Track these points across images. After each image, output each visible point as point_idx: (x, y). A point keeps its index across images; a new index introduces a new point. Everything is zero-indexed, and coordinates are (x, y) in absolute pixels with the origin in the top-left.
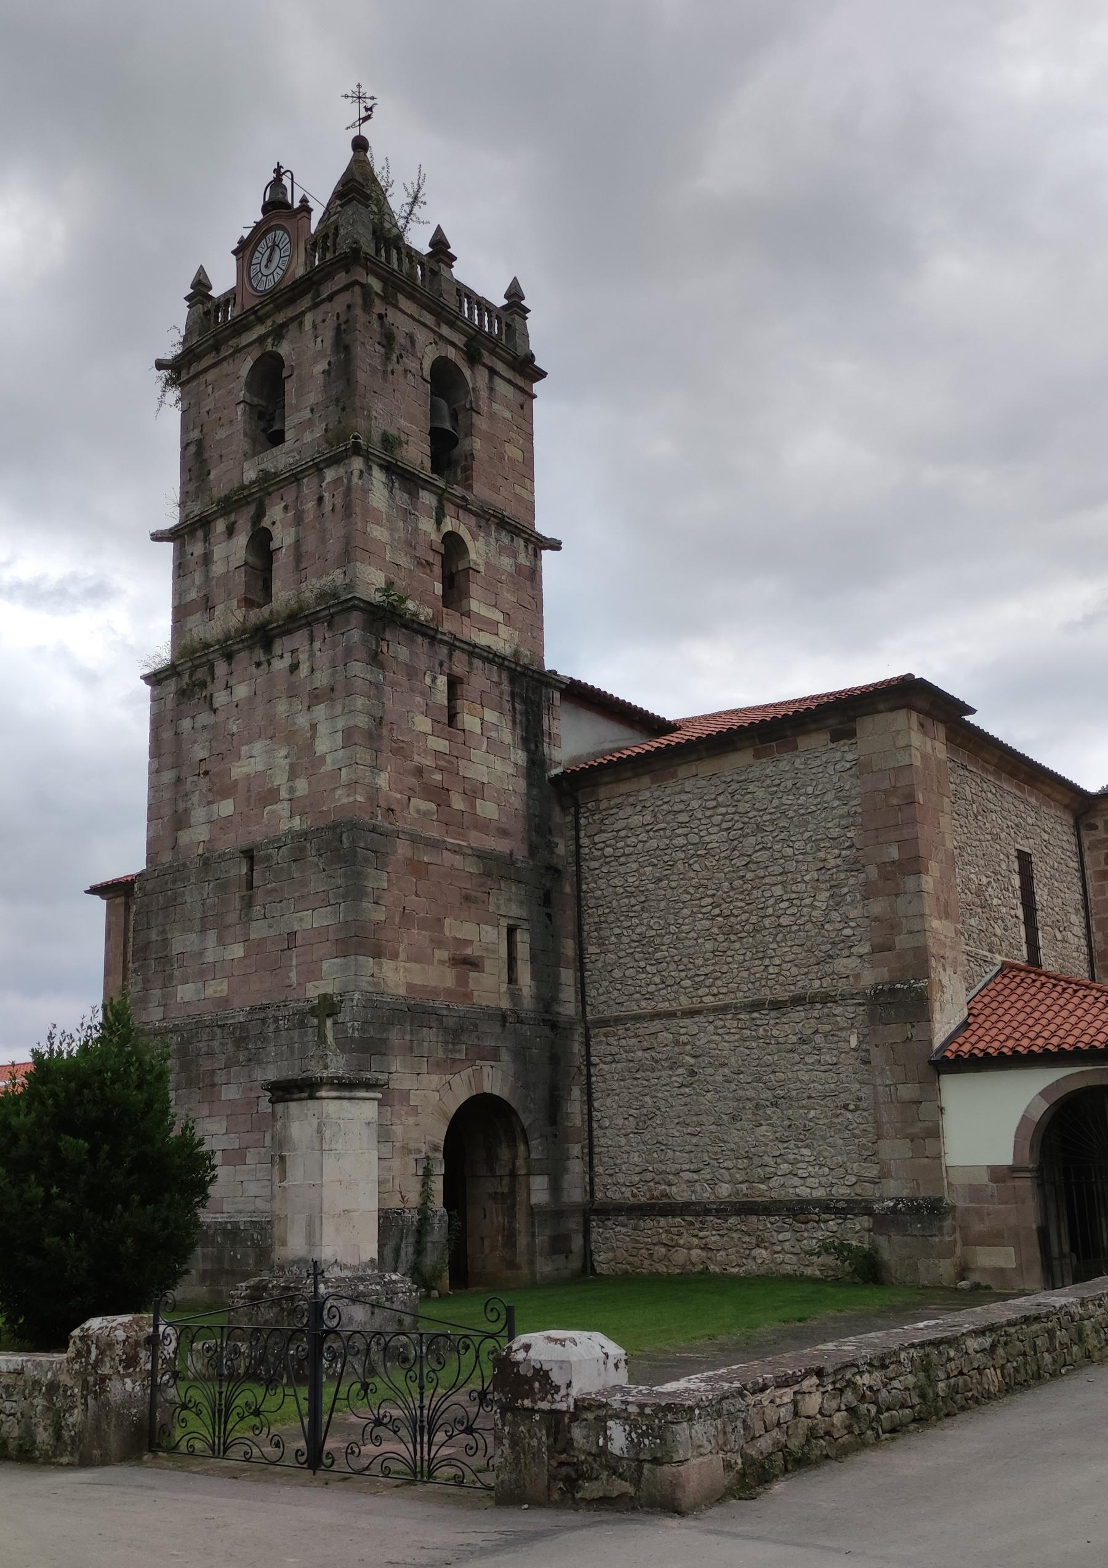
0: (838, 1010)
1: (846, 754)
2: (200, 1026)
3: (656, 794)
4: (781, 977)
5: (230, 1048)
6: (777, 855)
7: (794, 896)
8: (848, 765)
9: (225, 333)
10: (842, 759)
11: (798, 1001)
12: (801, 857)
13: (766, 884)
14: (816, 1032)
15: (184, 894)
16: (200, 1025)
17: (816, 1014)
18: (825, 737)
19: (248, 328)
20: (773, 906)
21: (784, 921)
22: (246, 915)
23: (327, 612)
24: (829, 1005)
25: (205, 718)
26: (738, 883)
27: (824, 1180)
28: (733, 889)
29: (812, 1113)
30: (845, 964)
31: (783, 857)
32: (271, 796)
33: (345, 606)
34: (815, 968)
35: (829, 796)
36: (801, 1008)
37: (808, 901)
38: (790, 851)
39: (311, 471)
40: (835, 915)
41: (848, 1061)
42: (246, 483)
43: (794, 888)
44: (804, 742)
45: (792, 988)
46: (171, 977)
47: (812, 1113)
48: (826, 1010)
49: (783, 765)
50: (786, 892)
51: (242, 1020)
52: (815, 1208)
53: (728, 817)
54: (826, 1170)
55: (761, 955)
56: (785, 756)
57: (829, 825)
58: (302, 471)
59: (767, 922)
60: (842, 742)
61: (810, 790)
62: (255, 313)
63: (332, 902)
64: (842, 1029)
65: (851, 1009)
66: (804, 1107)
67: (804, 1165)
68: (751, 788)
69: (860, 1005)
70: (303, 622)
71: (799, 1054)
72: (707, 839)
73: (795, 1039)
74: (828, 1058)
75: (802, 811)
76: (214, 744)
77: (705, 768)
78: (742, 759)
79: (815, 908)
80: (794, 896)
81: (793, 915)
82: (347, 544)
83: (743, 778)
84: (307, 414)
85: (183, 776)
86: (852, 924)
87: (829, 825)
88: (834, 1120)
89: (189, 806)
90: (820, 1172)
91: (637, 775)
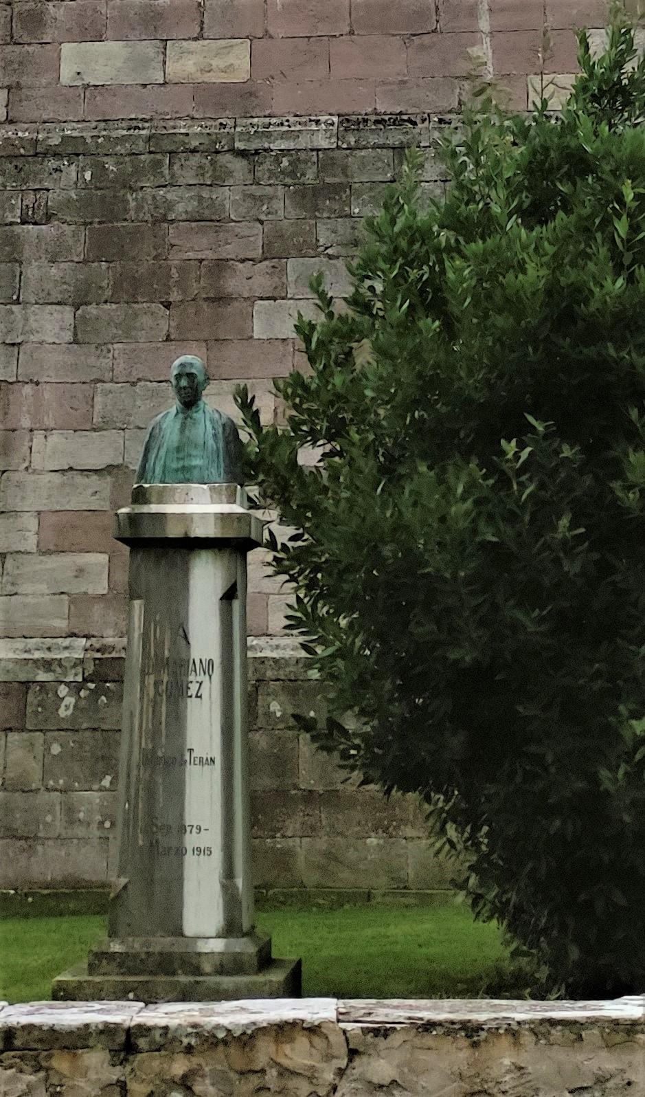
2: (165, 149)
5: (283, 210)
16: (167, 145)
51: (324, 144)
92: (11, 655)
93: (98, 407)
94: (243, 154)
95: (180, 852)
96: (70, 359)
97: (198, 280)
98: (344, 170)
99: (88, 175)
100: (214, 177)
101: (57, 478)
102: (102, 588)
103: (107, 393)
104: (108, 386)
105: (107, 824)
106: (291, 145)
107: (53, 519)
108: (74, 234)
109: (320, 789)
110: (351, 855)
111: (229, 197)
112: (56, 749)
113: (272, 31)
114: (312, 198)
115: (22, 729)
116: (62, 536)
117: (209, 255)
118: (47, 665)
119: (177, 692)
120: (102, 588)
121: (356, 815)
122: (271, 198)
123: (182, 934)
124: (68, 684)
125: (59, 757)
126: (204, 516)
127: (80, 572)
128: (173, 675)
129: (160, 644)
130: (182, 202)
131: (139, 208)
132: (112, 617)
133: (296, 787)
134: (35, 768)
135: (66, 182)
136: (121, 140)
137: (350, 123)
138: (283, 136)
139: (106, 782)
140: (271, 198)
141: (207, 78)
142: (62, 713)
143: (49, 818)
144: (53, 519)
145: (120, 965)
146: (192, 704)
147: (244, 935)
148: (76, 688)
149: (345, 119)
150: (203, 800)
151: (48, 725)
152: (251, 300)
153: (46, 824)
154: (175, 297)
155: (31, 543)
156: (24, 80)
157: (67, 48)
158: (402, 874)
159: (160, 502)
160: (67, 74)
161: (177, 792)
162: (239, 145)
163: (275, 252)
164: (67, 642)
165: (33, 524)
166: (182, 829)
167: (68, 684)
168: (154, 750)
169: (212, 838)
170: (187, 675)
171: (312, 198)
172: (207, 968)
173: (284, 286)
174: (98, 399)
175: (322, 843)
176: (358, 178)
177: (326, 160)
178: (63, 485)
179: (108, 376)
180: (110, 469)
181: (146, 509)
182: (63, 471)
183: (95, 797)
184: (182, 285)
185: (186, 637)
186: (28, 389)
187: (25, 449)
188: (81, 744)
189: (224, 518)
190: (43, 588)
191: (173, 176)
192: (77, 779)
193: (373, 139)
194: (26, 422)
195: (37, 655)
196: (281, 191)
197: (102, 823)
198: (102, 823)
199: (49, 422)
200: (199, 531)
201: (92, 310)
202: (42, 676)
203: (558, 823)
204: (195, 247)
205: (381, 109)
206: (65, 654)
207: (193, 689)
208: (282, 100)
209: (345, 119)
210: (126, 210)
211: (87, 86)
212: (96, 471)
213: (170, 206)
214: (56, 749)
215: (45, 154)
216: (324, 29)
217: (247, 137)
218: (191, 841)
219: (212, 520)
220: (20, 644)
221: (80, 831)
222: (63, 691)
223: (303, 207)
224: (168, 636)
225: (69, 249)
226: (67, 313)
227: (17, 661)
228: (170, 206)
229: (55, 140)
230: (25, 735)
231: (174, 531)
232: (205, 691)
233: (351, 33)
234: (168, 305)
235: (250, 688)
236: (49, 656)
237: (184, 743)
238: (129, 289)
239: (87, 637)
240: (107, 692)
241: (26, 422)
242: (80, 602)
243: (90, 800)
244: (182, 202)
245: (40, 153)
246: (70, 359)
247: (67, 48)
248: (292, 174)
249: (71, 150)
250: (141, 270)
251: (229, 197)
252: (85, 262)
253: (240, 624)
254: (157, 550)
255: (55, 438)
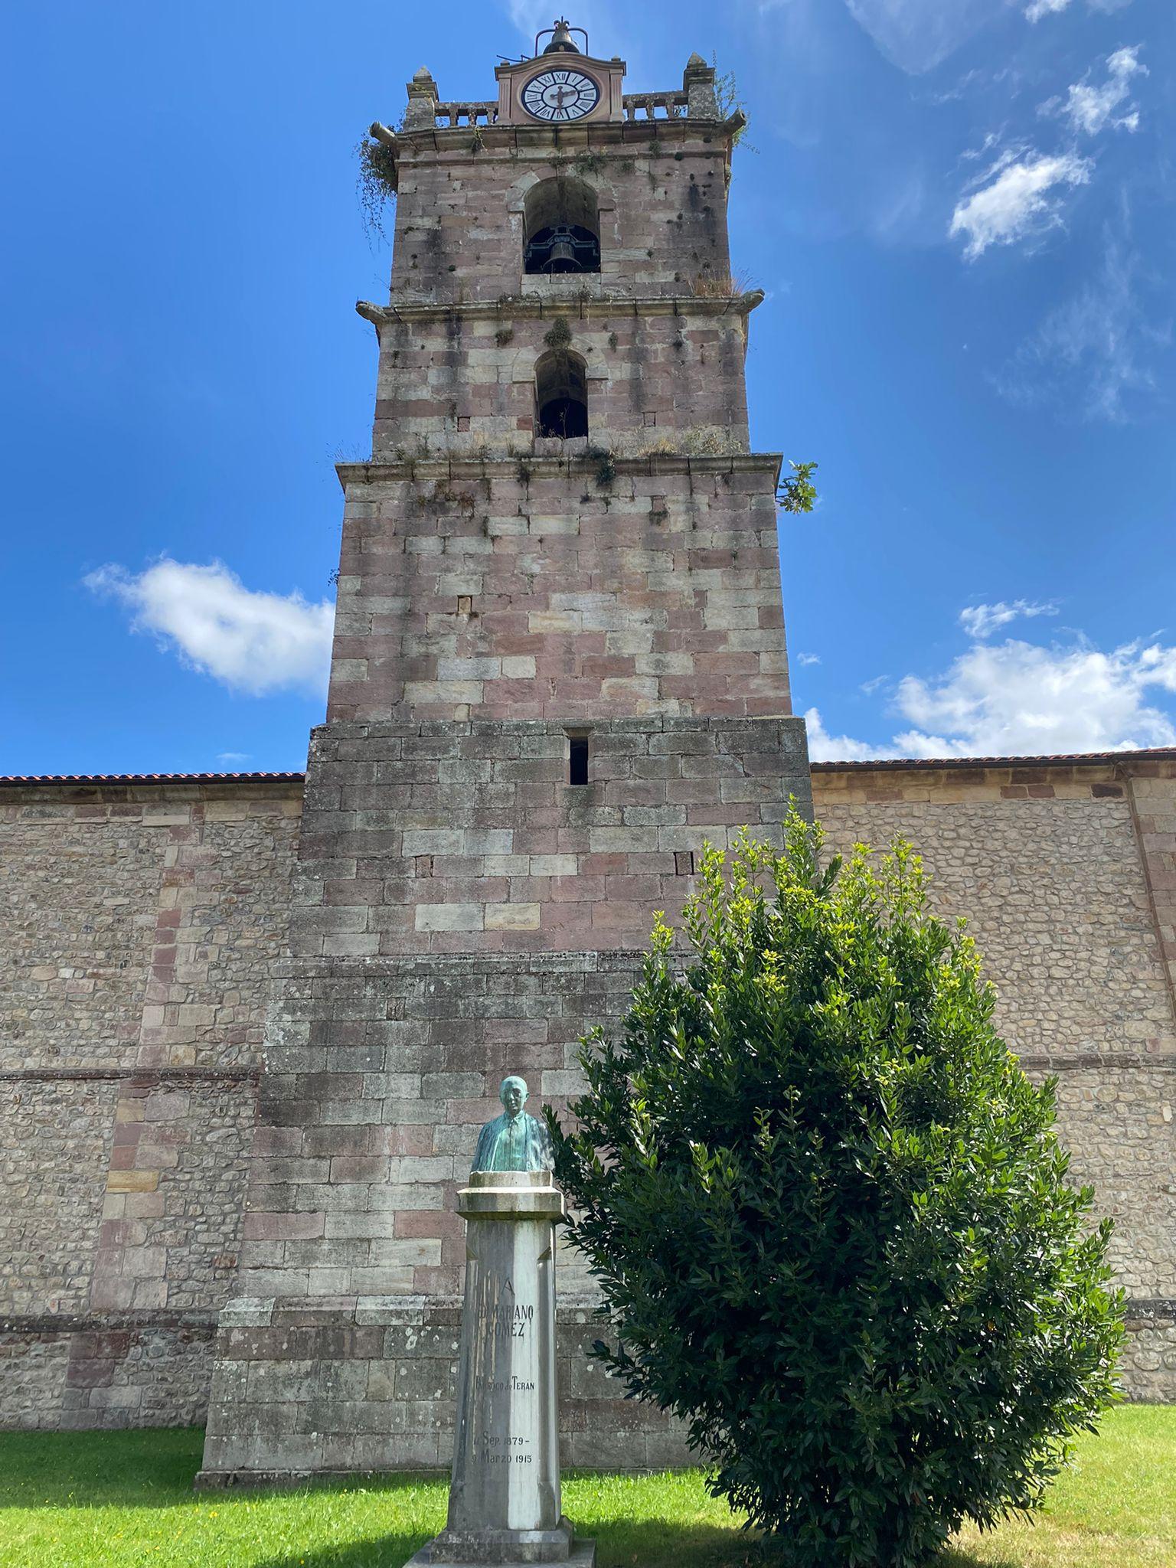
0: (1143, 1078)
1: (1112, 811)
2: (484, 970)
3: (874, 812)
4: (1059, 1035)
5: (562, 1012)
6: (1040, 901)
7: (1067, 947)
8: (1116, 823)
9: (498, 136)
10: (1109, 816)
11: (1091, 1061)
12: (1070, 908)
13: (1029, 930)
14: (1117, 1100)
15: (433, 770)
16: (485, 969)
17: (1115, 1079)
18: (1087, 791)
19: (532, 143)
20: (1040, 955)
21: (1056, 972)
22: (581, 816)
23: (728, 464)
24: (1131, 1070)
25: (467, 543)
26: (991, 925)
27: (1147, 1277)
28: (984, 930)
29: (1123, 1196)
30: (1135, 1028)
31: (1047, 904)
32: (623, 666)
33: (761, 463)
34: (1103, 1029)
35: (1096, 850)
36: (1095, 1071)
37: (1084, 955)
38: (1055, 899)
39: (665, 311)
40: (1119, 974)
41: (1162, 1136)
42: (524, 293)
43: (1065, 938)
44: (1061, 791)
45: (1075, 1048)
46: (399, 891)
47: (1123, 1196)
48: (1127, 1077)
49: (1037, 809)
50: (1055, 942)
51: (588, 969)
52: (1148, 1311)
53: (974, 852)
54: (1149, 1264)
55: (1031, 1007)
56: (1040, 800)
57: (1101, 879)
58: (648, 307)
59: (1035, 972)
60: (1107, 799)
61: (1074, 840)
62: (556, 131)
63: (766, 819)
64: (1149, 1099)
65: (1159, 1078)
66: (1111, 1187)
67: (1119, 1258)
68: (1001, 825)
69: (1168, 1073)
70: (681, 466)
71: (1098, 1125)
72: (949, 870)
73: (1090, 1106)
74: (1136, 1130)
75: (1065, 860)
76: (492, 581)
77: (941, 796)
78: (988, 794)
79: (1093, 963)
80: (1067, 947)
81: (1068, 967)
82: (731, 402)
83: (989, 813)
84: (642, 255)
85: (420, 608)
86: (1141, 985)
87: (1101, 879)
88: (1152, 1204)
89: (434, 649)
90: (1141, 1267)
91: (850, 787)
92: (374, 1308)
93: (436, 1141)
94: (535, 974)
95: (506, 1460)
96: (418, 1109)
97: (505, 1056)
98: (602, 986)
99: (432, 989)
100: (516, 990)
101: (407, 1189)
102: (437, 1262)
103: (441, 1132)
104: (443, 1127)
105: (438, 1424)
106: (567, 969)
107: (405, 1215)
108: (422, 1027)
109: (586, 1398)
110: (607, 1444)
111: (525, 1002)
112: (403, 1372)
113: (554, 897)
114: (579, 1004)
115: (380, 1358)
116: (411, 1226)
117: (511, 1040)
118: (398, 1314)
119: (505, 1332)
120: (437, 1262)
121: (610, 1415)
122: (553, 1004)
123: (507, 1528)
124: (413, 1327)
125: (406, 1377)
126: (526, 1196)
127: (422, 1251)
128: (503, 1315)
129: (490, 1295)
130: (495, 1006)
131: (466, 1010)
132: (443, 1281)
133: (569, 1397)
134: (389, 1385)
135: (420, 990)
136: (456, 965)
137: (605, 956)
138: (561, 963)
139: (438, 1394)
140: (553, 1004)
141: (512, 927)
142: (408, 1347)
143: (398, 1420)
144: (405, 1215)
145: (457, 1555)
146: (516, 1341)
147: (557, 1527)
148: (418, 1330)
149: (602, 953)
150: (525, 1418)
151: (398, 1352)
152: (540, 1070)
153: (396, 1424)
154: (489, 1068)
155: (389, 1232)
156: (391, 928)
157: (420, 908)
158: (642, 1457)
159: (491, 1185)
160: (419, 924)
161: (505, 1410)
162: (533, 969)
163: (556, 1037)
164: (412, 1299)
165: (390, 1219)
166: (507, 1441)
167: (413, 1327)
168: (485, 1378)
169: (532, 1448)
170: (512, 1318)
171: (579, 1004)
172: (528, 1556)
173: (562, 1061)
174: (436, 1136)
175: (587, 1436)
176: (612, 991)
177: (590, 980)
178: (411, 1193)
179: (443, 1120)
180: (443, 1182)
181: (481, 1190)
182: (411, 1184)
183: (430, 1405)
184: (494, 1061)
185: (511, 1289)
186: (389, 1129)
187: (386, 1169)
188: (421, 1368)
189: (541, 1197)
190: (396, 1262)
191: (489, 989)
192: (418, 1393)
193: (620, 966)
194: (387, 1151)
195: (392, 1307)
196: (560, 999)
197: (434, 1423)
198: (434, 1423)
199: (402, 1151)
200: (522, 1207)
201: (433, 1076)
202: (395, 1322)
203: (810, 1435)
204: (505, 1036)
205: (625, 947)
206: (411, 1307)
207: (517, 1329)
208: (560, 940)
209: (602, 953)
210: (457, 1011)
211: (432, 933)
212: (434, 1184)
213: (486, 1008)
214: (403, 1372)
215: (404, 975)
216: (588, 897)
217: (536, 963)
218: (515, 1450)
219: (532, 1199)
220: (379, 1300)
221: (420, 1429)
222: (409, 1331)
223: (574, 1009)
224: (497, 1286)
225: (418, 1037)
226: (417, 1080)
227: (377, 1312)
228: (486, 1008)
229: (411, 966)
230: (382, 1362)
231: (502, 1207)
232: (526, 1331)
233: (606, 899)
234: (484, 1073)
235: (565, 1330)
236: (399, 1308)
237: (509, 1372)
238: (458, 1062)
239: (427, 1295)
240: (439, 1333)
241: (387, 1151)
242: (422, 1272)
243: (427, 1406)
244: (495, 1006)
245: (400, 974)
246: (418, 1109)
247: (420, 908)
248: (568, 988)
249: (423, 972)
250: (467, 1050)
251: (525, 1002)
252: (429, 1045)
253: (551, 1277)
254: (491, 1221)
255: (407, 1161)
